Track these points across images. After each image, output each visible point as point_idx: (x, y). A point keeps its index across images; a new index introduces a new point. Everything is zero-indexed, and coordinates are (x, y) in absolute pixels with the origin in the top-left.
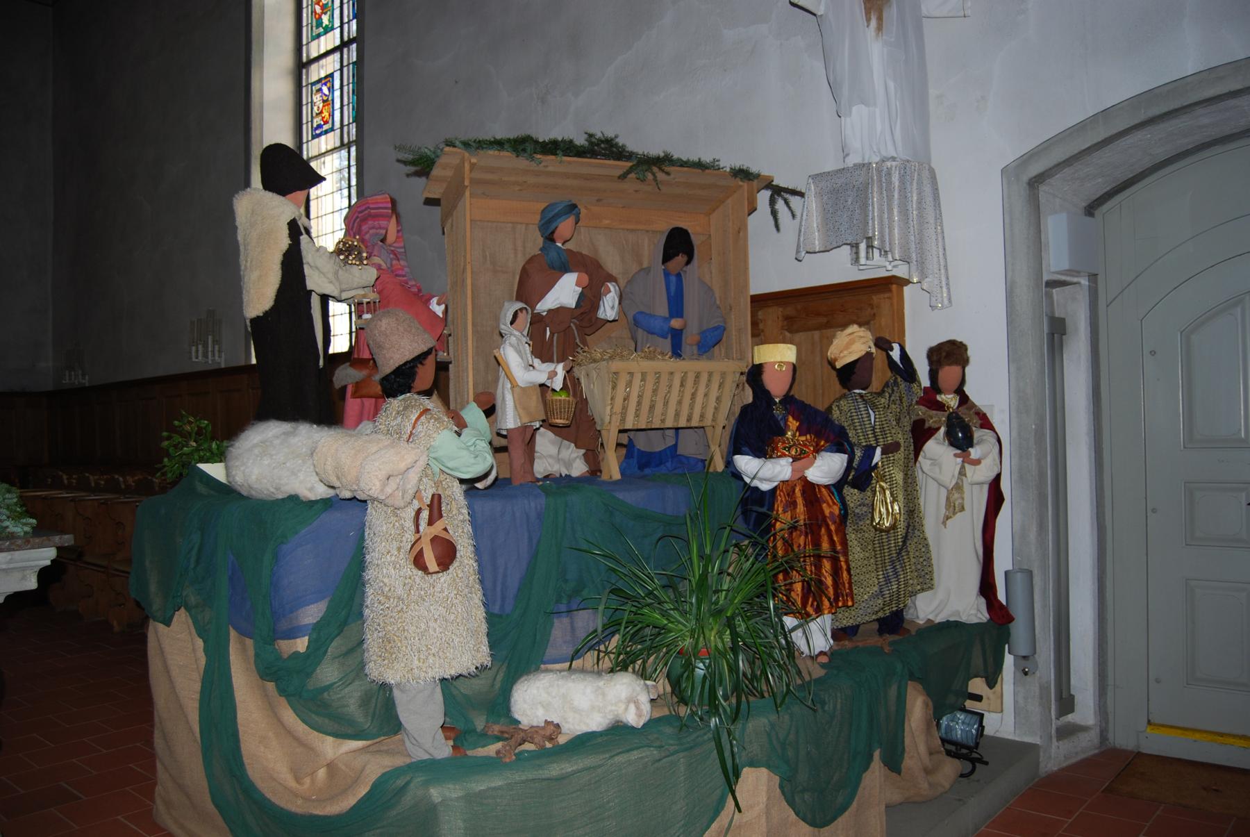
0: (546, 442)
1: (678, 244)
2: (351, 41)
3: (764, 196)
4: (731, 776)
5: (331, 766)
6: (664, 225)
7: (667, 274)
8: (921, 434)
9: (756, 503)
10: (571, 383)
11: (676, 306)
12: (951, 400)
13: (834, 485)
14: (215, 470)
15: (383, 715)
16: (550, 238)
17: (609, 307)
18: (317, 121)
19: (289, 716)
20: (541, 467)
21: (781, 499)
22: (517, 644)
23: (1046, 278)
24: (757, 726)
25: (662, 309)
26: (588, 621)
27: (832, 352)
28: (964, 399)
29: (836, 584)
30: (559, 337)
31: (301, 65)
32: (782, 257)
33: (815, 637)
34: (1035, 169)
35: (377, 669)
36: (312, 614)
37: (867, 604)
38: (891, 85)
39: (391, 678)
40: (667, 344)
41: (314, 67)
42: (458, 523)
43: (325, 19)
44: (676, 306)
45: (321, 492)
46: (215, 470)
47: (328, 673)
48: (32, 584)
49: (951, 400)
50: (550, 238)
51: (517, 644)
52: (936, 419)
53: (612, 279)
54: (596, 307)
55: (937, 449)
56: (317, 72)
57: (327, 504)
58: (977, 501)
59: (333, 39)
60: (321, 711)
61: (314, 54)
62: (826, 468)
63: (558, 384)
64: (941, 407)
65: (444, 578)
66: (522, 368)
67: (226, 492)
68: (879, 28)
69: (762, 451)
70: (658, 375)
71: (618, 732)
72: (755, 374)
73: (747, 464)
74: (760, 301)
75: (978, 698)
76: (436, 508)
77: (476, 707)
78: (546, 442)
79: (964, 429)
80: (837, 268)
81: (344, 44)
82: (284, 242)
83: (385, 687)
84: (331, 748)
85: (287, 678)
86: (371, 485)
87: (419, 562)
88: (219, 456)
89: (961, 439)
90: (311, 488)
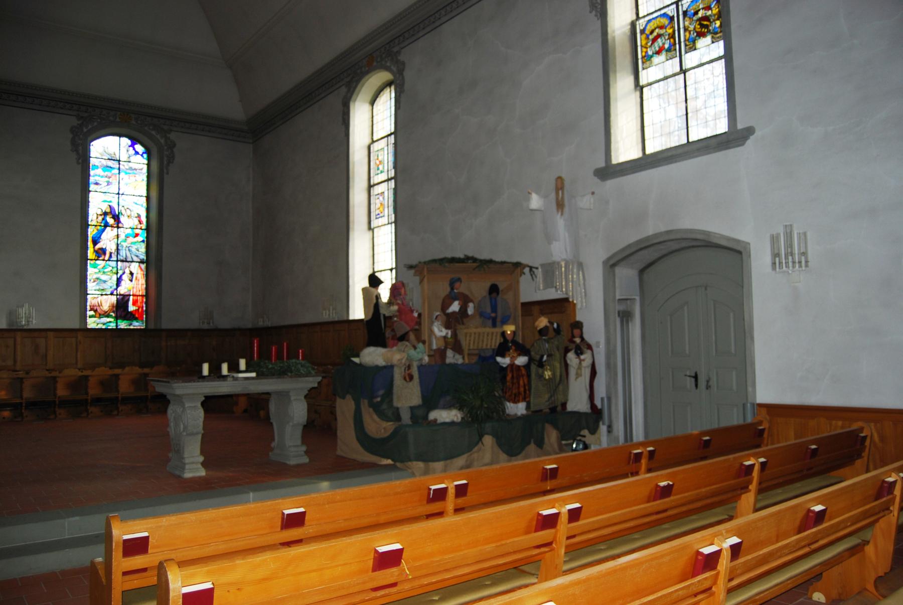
0: (450, 353)
1: (494, 290)
2: (392, 179)
3: (527, 270)
4: (481, 436)
5: (384, 428)
6: (488, 285)
7: (491, 299)
8: (567, 350)
9: (503, 370)
10: (455, 335)
11: (494, 308)
12: (578, 340)
13: (524, 366)
14: (356, 360)
15: (397, 417)
16: (452, 289)
17: (470, 310)
18: (378, 212)
19: (375, 417)
20: (448, 361)
21: (509, 369)
22: (430, 401)
23: (618, 297)
24: (488, 426)
25: (489, 310)
26: (448, 398)
27: (537, 323)
28: (583, 339)
29: (525, 392)
30: (451, 321)
31: (370, 187)
32: (532, 290)
33: (518, 409)
34: (612, 262)
35: (396, 404)
36: (381, 392)
37: (541, 401)
38: (567, 235)
39: (399, 405)
40: (490, 322)
41: (376, 187)
42: (415, 372)
43: (381, 167)
44: (494, 308)
45: (384, 364)
46: (356, 360)
47: (384, 406)
48: (316, 385)
49: (578, 340)
50: (452, 289)
51: (430, 401)
52: (572, 346)
53: (472, 301)
54: (466, 310)
55: (571, 356)
56: (377, 190)
57: (385, 367)
58: (587, 373)
59: (383, 177)
60: (382, 415)
61: (376, 182)
62: (521, 360)
63: (449, 336)
64: (574, 342)
65: (411, 384)
66: (440, 331)
67: (360, 365)
68: (562, 214)
69: (503, 356)
70: (479, 334)
71: (453, 423)
72: (503, 334)
73: (499, 359)
74: (524, 305)
75: (584, 436)
76: (409, 367)
77: (419, 416)
78: (450, 353)
79: (582, 347)
80: (552, 294)
81: (388, 180)
82: (375, 301)
83: (398, 409)
84: (385, 424)
85: (376, 408)
86: (395, 361)
87: (405, 379)
88: (358, 356)
89: (579, 352)
90: (381, 362)
